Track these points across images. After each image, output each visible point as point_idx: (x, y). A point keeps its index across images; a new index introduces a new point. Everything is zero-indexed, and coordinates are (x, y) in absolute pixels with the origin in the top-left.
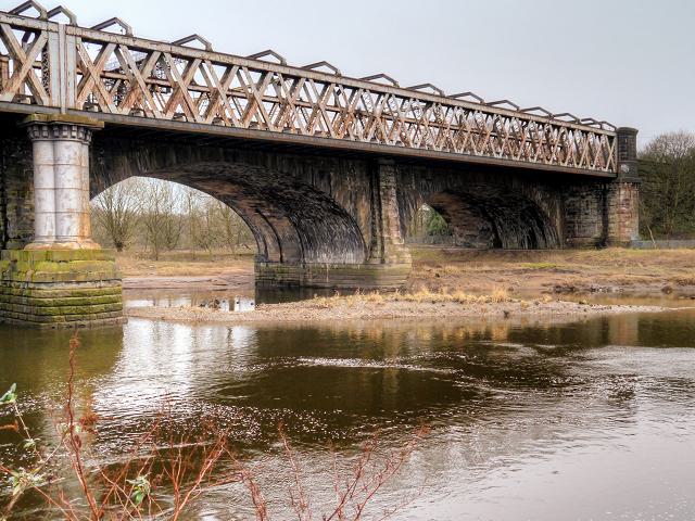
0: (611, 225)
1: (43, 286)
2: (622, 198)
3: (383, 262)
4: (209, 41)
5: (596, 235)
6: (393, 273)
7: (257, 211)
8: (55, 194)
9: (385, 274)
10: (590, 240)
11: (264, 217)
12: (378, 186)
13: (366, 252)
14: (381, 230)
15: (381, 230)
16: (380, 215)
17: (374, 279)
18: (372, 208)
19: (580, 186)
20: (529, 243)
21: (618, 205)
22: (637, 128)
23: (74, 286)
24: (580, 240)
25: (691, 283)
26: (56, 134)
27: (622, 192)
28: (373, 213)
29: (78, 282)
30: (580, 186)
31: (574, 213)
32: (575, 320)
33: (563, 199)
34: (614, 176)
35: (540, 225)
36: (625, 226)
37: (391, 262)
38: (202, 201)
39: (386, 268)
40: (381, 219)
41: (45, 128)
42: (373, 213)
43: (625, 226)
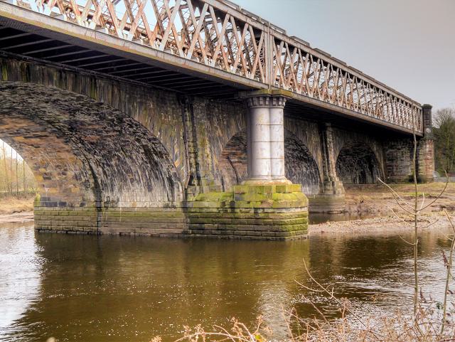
0: (420, 168)
1: (284, 211)
2: (427, 150)
3: (334, 193)
4: (308, 42)
5: (409, 174)
6: (340, 200)
7: (228, 158)
8: (271, 145)
9: (336, 201)
10: (405, 177)
11: (231, 163)
12: (326, 141)
13: (321, 186)
14: (329, 171)
15: (329, 171)
16: (328, 161)
17: (328, 205)
18: (323, 156)
19: (397, 141)
20: (360, 180)
21: (425, 154)
22: (431, 104)
23: (299, 210)
24: (397, 177)
25: (2, 212)
26: (274, 103)
27: (428, 146)
28: (324, 160)
29: (301, 208)
30: (397, 141)
31: (392, 160)
32: (394, 234)
33: (384, 150)
34: (422, 135)
35: (371, 168)
36: (429, 168)
37: (339, 193)
38: (20, 159)
39: (336, 197)
40: (328, 164)
41: (268, 99)
42: (324, 160)
43: (429, 168)
